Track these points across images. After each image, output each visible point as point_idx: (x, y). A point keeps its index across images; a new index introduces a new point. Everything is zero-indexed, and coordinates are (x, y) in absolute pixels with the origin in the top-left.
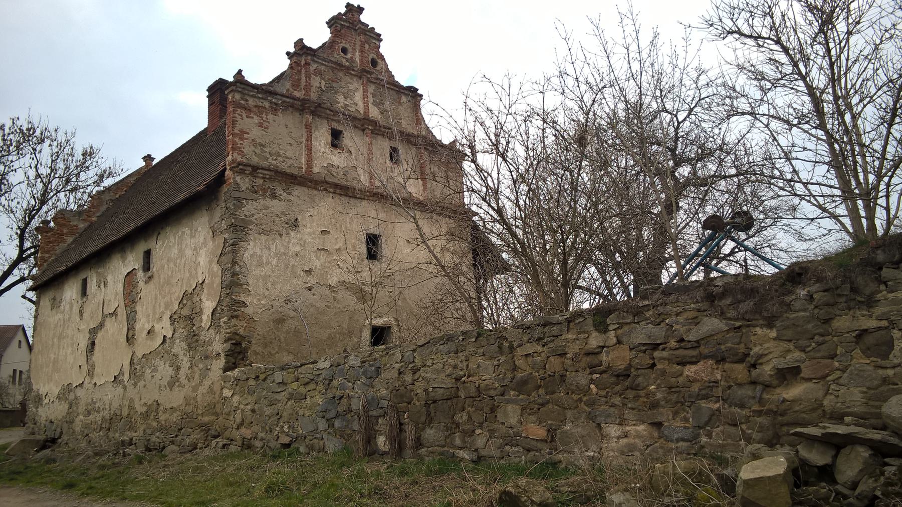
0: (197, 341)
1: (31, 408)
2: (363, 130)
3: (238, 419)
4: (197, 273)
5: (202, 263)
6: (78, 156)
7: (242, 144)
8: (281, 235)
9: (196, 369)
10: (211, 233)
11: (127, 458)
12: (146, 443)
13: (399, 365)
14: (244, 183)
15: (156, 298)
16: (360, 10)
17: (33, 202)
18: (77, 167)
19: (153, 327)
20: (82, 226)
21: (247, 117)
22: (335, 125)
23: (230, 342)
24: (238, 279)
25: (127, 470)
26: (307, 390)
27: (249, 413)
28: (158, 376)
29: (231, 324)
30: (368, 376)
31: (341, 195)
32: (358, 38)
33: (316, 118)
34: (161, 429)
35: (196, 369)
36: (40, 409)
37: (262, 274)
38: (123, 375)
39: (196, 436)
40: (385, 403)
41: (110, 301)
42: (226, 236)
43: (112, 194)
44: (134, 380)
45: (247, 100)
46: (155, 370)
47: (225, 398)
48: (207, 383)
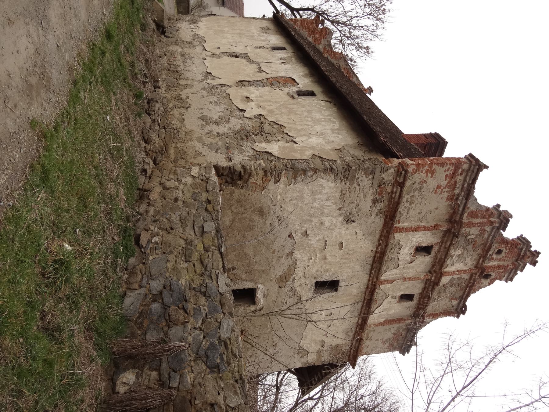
0: (242, 139)
1: (187, 18)
2: (430, 272)
3: (169, 184)
4: (301, 136)
5: (311, 140)
6: (365, 44)
7: (422, 171)
8: (340, 209)
9: (218, 139)
10: (338, 148)
11: (140, 85)
12: (155, 99)
13: (222, 402)
14: (389, 176)
15: (276, 102)
16: (534, 263)
17: (333, 15)
18: (358, 44)
19: (252, 101)
20: (321, 47)
21: (446, 176)
22: (435, 249)
23: (242, 170)
24: (301, 175)
25: (127, 85)
26: (195, 262)
27: (175, 195)
28: (211, 107)
29: (259, 171)
30: (209, 353)
31: (374, 257)
32: (509, 263)
33: (443, 233)
34: (166, 111)
35: (218, 139)
36: (187, 23)
37: (305, 195)
38: (212, 79)
39: (157, 142)
40: (175, 384)
41: (271, 67)
42: (339, 162)
43: (344, 66)
44: (208, 87)
45: (461, 174)
46: (216, 104)
47: (190, 169)
48: (205, 150)
